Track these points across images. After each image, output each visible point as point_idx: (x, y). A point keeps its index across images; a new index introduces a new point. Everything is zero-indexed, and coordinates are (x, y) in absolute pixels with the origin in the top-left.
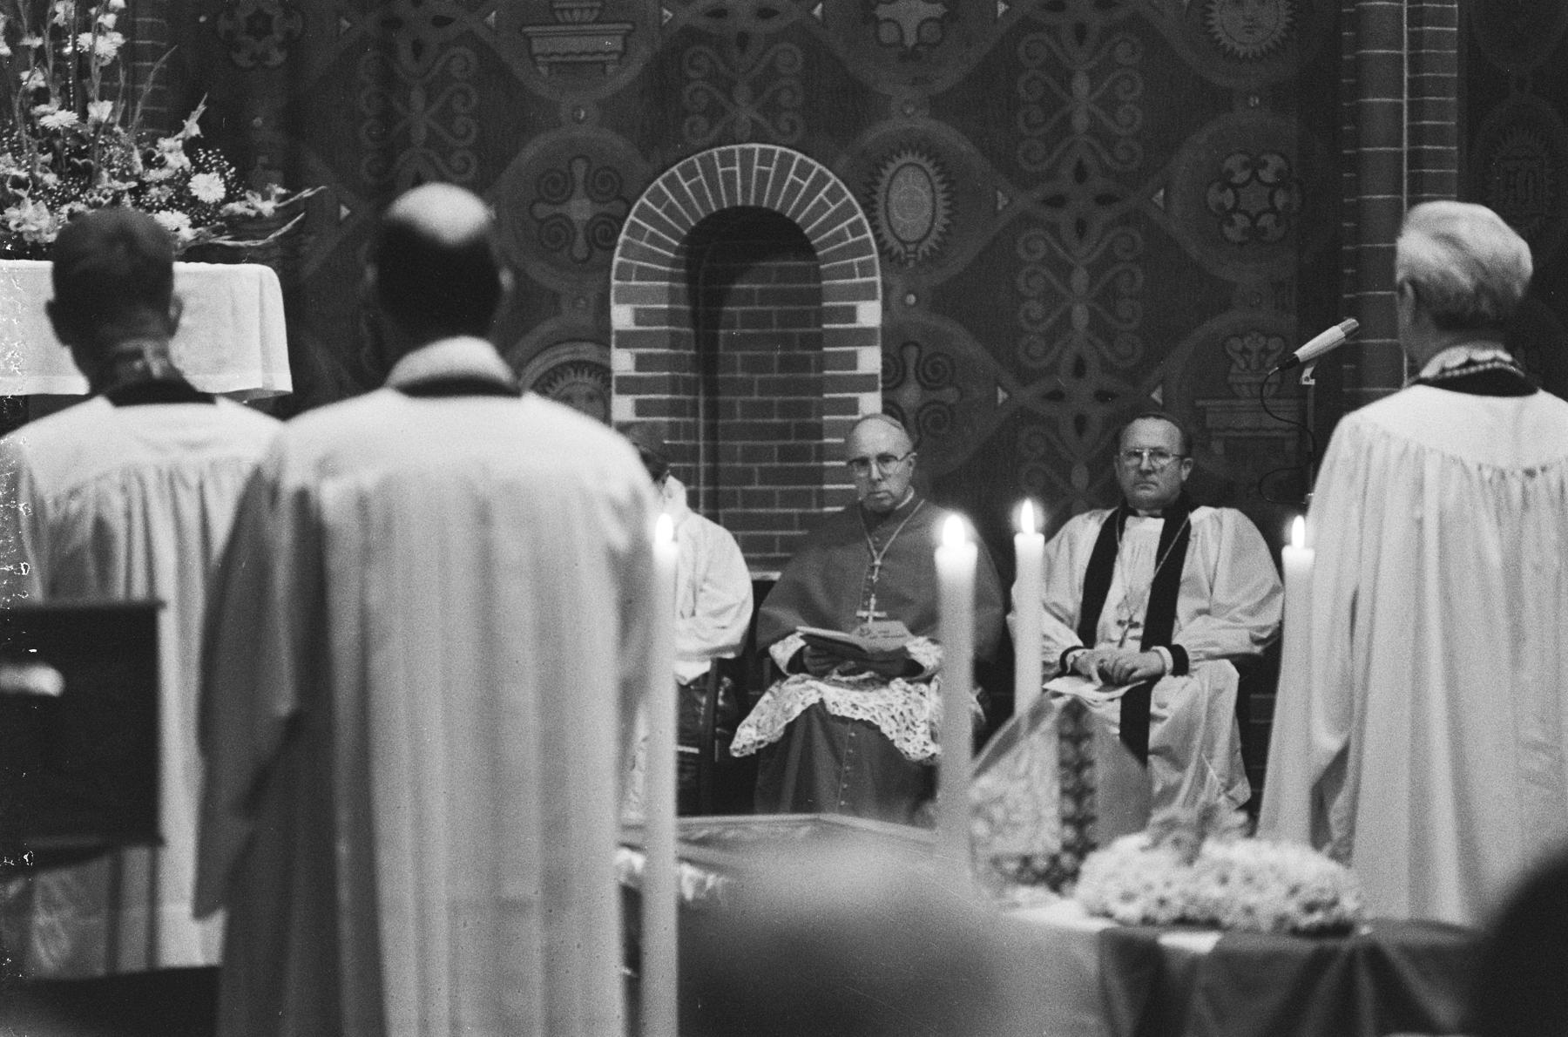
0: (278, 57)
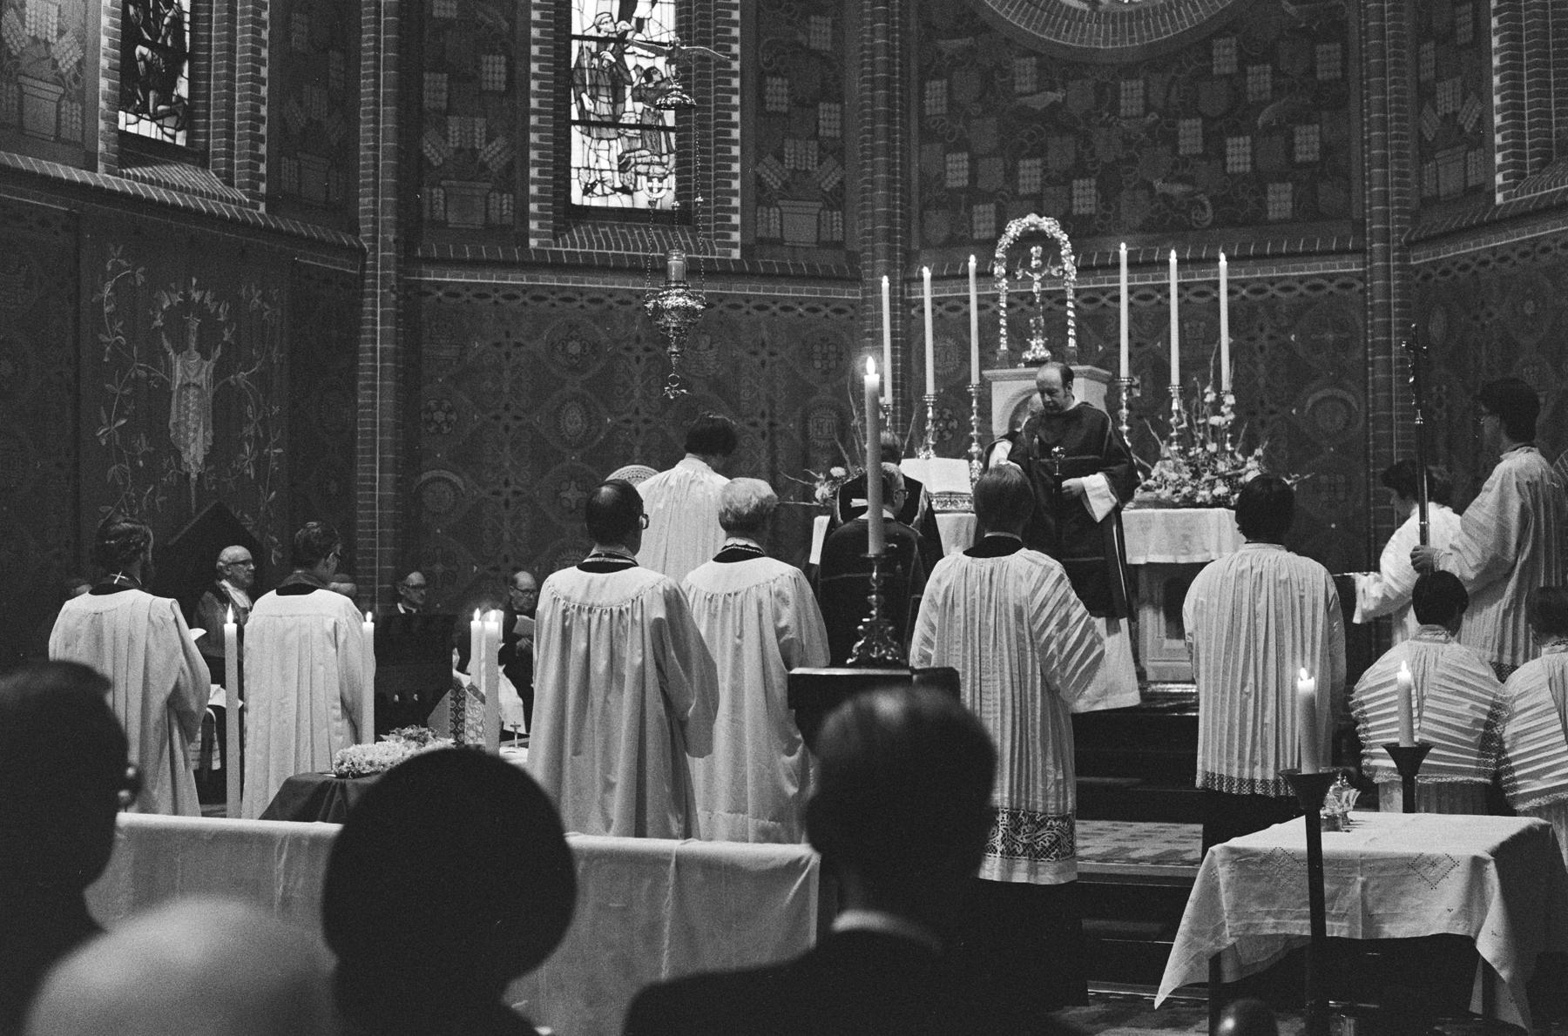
0: (1445, 415)
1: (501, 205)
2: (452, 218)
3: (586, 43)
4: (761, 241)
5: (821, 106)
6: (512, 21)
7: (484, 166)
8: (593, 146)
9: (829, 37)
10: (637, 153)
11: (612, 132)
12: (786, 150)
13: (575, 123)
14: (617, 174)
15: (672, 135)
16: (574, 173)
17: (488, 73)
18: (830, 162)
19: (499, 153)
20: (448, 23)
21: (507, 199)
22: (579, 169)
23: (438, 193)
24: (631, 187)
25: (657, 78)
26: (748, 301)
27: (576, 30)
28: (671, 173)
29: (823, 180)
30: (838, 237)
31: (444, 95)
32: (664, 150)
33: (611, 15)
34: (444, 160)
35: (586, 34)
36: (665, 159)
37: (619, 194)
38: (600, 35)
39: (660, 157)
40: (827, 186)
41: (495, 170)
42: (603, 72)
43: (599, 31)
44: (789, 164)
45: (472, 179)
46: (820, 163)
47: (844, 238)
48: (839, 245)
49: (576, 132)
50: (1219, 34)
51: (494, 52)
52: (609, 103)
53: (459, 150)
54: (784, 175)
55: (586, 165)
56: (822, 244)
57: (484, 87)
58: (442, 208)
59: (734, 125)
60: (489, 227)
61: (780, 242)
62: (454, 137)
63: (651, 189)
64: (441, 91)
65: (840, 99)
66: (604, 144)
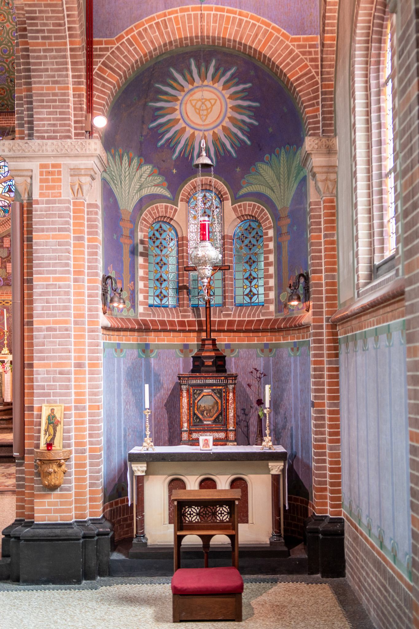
50: (5, 236)
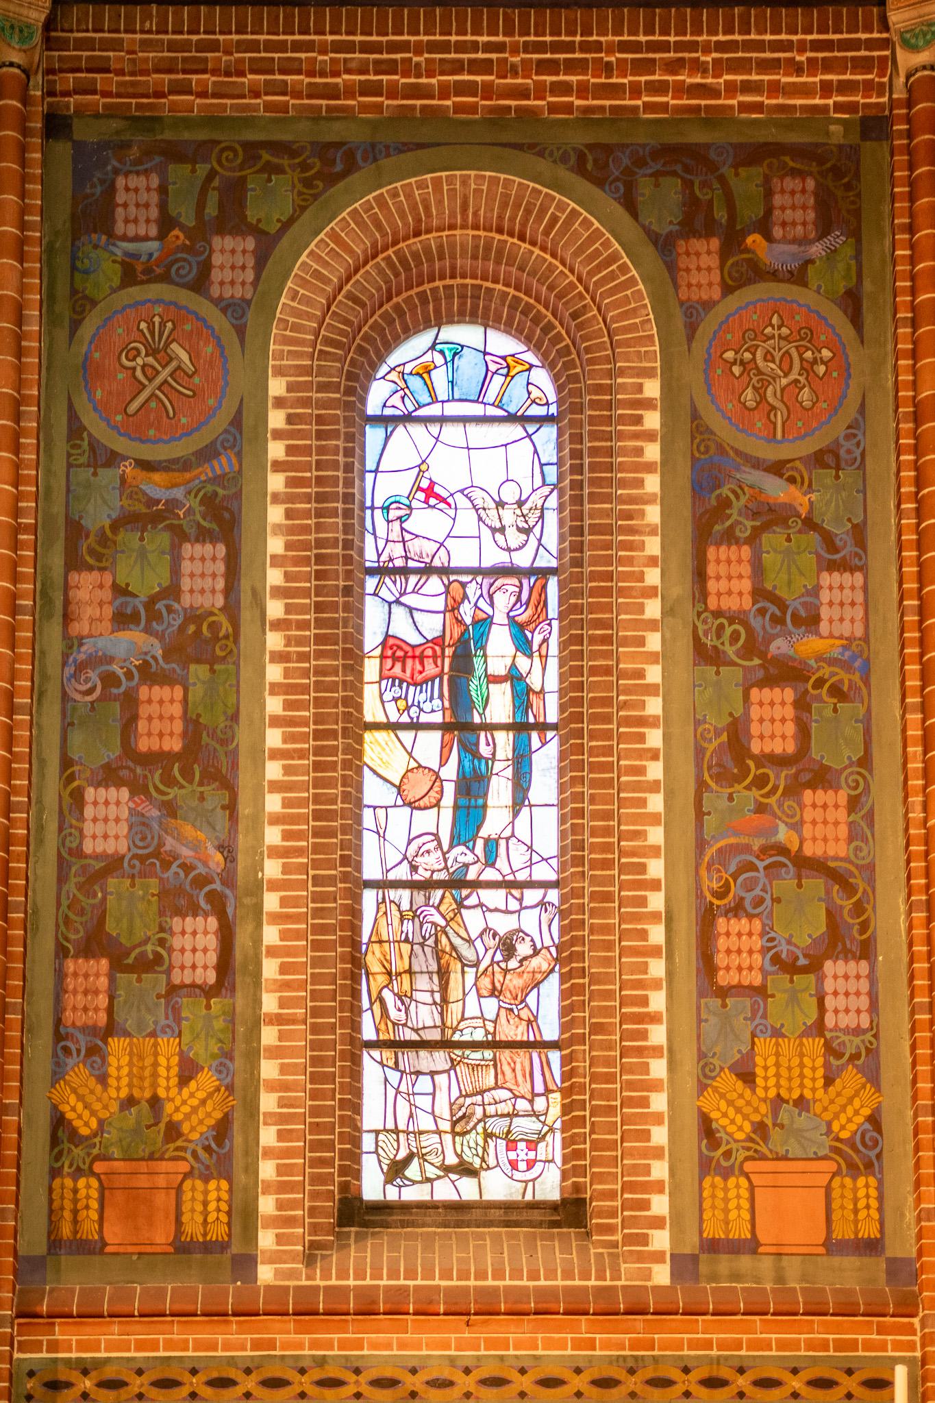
1: (205, 1204)
2: (114, 1234)
3: (393, 894)
4: (713, 1246)
5: (828, 966)
6: (228, 850)
7: (173, 1131)
8: (403, 1088)
9: (843, 831)
10: (488, 1097)
11: (439, 1059)
12: (759, 1060)
13: (370, 1045)
14: (448, 1138)
15: (555, 1057)
16: (368, 1142)
17: (183, 950)
18: (851, 1079)
19: (203, 1102)
20: (113, 864)
21: (217, 1189)
22: (377, 1132)
23: (88, 1187)
24: (477, 1162)
25: (523, 949)
26: (686, 1370)
27: (371, 871)
28: (551, 1129)
29: (836, 1116)
30: (869, 1230)
31: (102, 1000)
32: (539, 1088)
33: (436, 836)
34: (101, 1123)
35: (392, 876)
36: (540, 1104)
37: (453, 1177)
38: (416, 877)
39: (531, 1102)
40: (843, 1128)
41: (195, 1136)
42: (422, 945)
43: (414, 869)
44: (766, 1089)
45: (151, 1158)
46: (829, 1081)
47: (882, 1231)
48: (872, 1247)
49: (372, 1070)
51: (195, 911)
52: (435, 1003)
53: (130, 1102)
54: (756, 1110)
55: (390, 1125)
56: (832, 1246)
57: (177, 978)
58: (95, 1216)
59: (654, 1018)
60: (182, 1248)
61: (752, 1246)
62: (118, 1079)
63: (514, 1165)
64: (96, 992)
65: (866, 951)
66: (424, 1084)
